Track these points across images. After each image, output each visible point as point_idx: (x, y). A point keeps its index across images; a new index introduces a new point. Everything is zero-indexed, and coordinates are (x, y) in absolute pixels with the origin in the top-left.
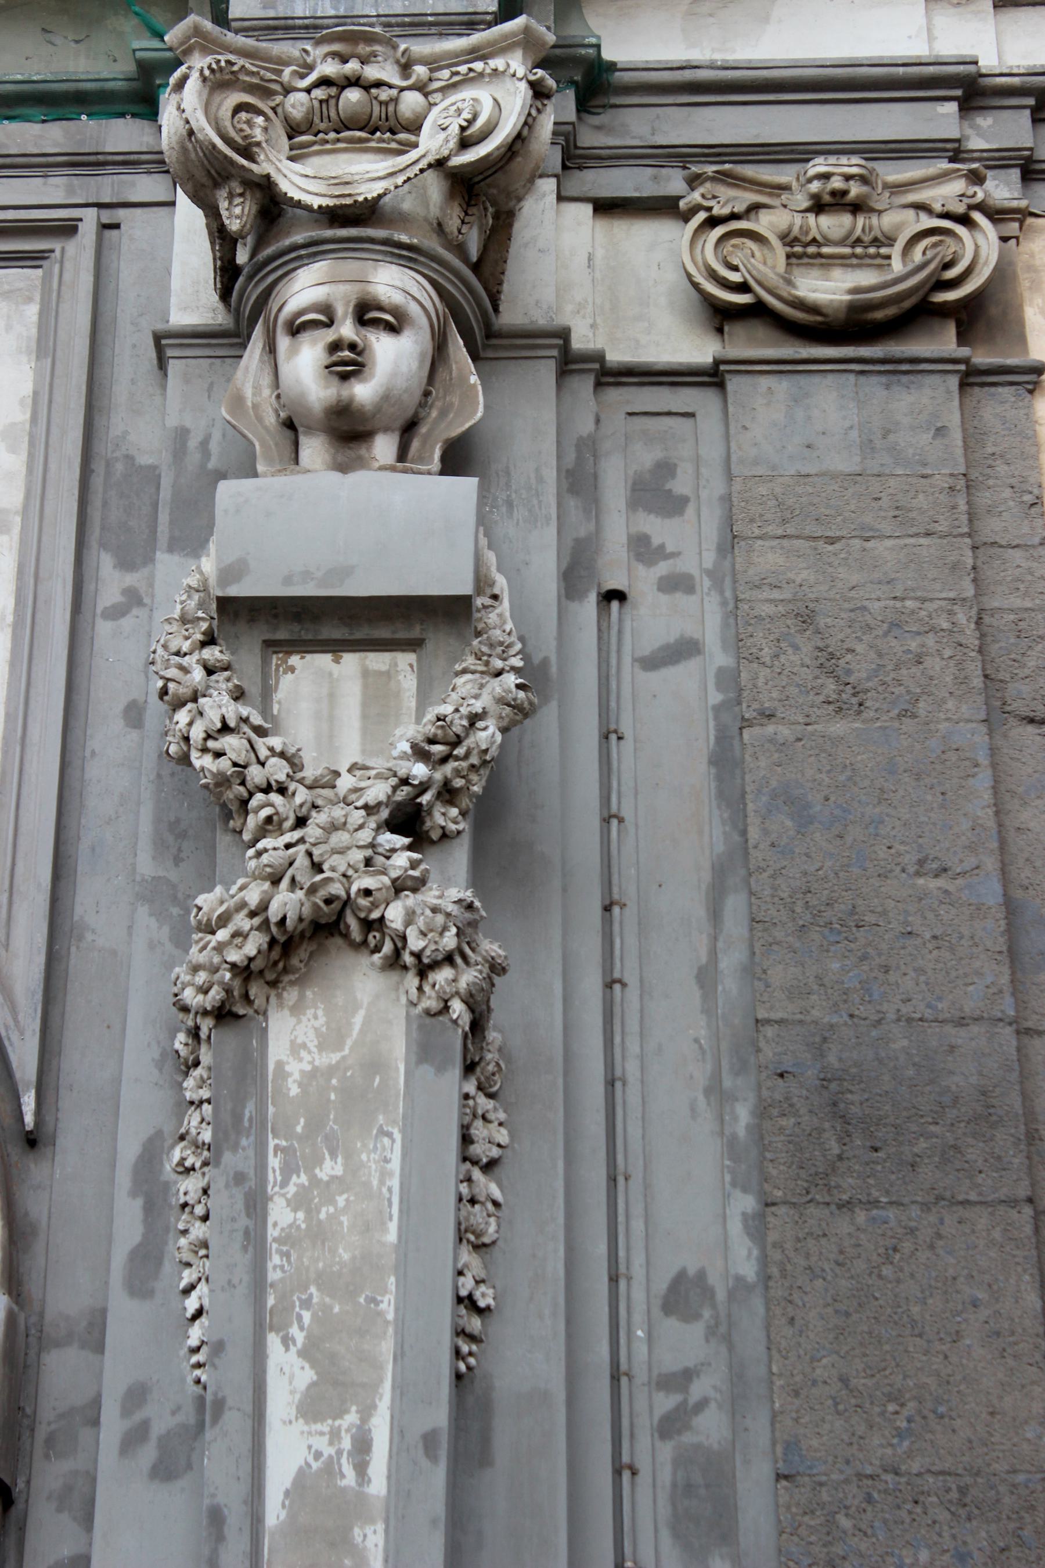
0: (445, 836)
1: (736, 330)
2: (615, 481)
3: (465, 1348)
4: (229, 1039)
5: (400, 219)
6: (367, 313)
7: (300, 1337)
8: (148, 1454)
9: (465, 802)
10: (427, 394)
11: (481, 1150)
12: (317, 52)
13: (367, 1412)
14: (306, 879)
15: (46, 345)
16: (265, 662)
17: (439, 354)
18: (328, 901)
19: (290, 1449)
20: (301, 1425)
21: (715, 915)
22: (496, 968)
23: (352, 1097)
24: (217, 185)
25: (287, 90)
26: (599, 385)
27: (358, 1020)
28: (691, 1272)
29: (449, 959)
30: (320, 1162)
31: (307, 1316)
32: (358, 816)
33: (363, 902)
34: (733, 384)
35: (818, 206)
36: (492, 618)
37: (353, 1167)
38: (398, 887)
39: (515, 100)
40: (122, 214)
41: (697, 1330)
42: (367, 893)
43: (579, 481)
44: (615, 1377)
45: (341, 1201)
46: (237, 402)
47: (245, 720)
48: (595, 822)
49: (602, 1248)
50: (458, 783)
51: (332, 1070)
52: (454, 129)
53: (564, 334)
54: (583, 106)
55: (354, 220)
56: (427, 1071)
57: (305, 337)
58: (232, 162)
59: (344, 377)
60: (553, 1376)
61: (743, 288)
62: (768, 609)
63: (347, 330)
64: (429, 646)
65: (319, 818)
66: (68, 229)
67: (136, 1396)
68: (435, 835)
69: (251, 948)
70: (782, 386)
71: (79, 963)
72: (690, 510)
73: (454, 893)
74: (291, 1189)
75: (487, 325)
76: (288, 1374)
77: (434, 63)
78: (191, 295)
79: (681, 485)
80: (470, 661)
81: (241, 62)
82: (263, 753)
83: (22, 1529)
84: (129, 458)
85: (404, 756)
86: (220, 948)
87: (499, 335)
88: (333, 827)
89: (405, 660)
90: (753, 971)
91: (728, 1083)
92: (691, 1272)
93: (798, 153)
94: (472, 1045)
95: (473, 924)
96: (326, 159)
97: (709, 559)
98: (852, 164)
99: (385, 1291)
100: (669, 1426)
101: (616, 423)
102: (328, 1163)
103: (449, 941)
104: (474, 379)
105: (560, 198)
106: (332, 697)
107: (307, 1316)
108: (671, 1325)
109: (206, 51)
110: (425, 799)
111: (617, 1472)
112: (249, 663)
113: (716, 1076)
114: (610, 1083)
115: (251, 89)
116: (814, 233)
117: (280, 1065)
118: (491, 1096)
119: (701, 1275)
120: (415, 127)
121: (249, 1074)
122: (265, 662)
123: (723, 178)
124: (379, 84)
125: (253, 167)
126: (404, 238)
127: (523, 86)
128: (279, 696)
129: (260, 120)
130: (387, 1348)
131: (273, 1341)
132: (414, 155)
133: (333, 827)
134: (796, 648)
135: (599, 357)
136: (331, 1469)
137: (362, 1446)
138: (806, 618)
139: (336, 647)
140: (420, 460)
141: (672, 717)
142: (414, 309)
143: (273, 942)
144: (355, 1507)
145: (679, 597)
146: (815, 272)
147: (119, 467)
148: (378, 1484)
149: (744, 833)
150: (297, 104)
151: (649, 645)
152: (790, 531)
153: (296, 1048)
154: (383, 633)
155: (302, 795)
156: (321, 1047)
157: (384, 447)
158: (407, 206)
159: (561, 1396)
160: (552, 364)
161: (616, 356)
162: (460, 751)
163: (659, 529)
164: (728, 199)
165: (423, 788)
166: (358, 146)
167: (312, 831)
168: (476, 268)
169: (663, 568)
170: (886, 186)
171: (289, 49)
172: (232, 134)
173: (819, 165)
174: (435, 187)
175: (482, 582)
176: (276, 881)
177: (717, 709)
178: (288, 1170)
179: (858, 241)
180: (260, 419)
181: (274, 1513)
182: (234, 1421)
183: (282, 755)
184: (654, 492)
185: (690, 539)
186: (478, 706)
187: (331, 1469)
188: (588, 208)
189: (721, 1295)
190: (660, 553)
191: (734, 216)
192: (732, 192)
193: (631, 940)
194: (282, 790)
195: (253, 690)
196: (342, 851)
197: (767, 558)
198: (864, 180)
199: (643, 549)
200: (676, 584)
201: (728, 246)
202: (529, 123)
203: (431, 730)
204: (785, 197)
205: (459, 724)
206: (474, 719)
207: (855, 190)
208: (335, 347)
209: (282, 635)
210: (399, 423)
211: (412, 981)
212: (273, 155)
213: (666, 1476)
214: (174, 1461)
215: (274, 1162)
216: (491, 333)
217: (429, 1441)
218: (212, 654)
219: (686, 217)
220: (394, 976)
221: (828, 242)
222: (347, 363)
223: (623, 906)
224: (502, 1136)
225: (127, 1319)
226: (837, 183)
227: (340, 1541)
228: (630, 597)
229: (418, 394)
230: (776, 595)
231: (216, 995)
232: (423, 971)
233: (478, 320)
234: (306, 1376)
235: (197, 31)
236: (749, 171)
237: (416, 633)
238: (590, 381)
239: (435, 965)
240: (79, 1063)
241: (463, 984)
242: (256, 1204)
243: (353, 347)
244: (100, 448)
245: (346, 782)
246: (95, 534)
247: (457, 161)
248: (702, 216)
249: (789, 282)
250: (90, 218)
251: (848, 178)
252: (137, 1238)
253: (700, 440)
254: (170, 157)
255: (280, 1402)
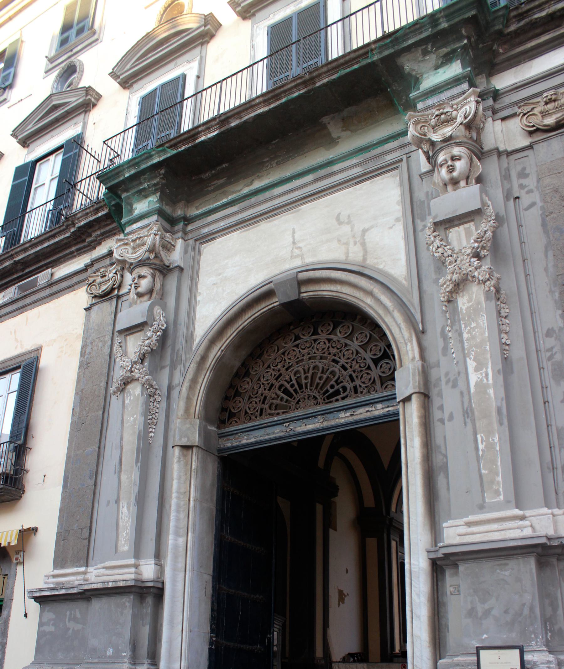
0: (485, 256)
1: (534, 135)
2: (514, 174)
3: (506, 353)
4: (451, 305)
5: (457, 137)
6: (453, 158)
7: (472, 357)
8: (450, 384)
9: (488, 248)
10: (470, 170)
11: (504, 314)
12: (434, 110)
13: (487, 369)
14: (458, 271)
15: (401, 184)
16: (445, 232)
17: (471, 160)
18: (464, 275)
19: (473, 378)
20: (475, 373)
21: (546, 256)
22: (498, 279)
23: (475, 311)
24: (421, 143)
25: (431, 120)
26: (508, 156)
27: (474, 296)
28: (550, 328)
29: (488, 280)
30: (471, 324)
31: (473, 353)
32: (466, 257)
33: (470, 273)
34: (535, 147)
35: (546, 103)
36: (488, 210)
37: (478, 324)
38: (476, 269)
39: (473, 105)
40: (411, 154)
41: (553, 339)
42: (471, 271)
43: (506, 176)
44: (537, 352)
45: (476, 330)
46: (434, 184)
47: (442, 245)
48: (519, 244)
49: (531, 328)
50: (485, 245)
51: (471, 306)
52: (463, 116)
53: (497, 149)
54: (495, 100)
55: (448, 141)
56: (488, 302)
57: (443, 167)
58: (421, 138)
59: (451, 172)
60: (523, 354)
61: (533, 126)
62: (549, 191)
63: (450, 163)
64: (476, 220)
65: (459, 259)
66: (401, 160)
67: (447, 374)
68: (483, 256)
69: (450, 288)
70: (545, 144)
71: (426, 297)
72: (530, 176)
73: (487, 267)
74: (467, 330)
75: (481, 152)
76: (471, 364)
77: (457, 104)
78: (425, 166)
79: (527, 171)
80: (484, 220)
81: (420, 118)
82: (446, 250)
83: (432, 401)
84: (420, 200)
85: (473, 243)
86: (445, 289)
87: (484, 153)
88: (462, 260)
89: (472, 224)
90: (556, 266)
91: (553, 289)
92: (550, 328)
93: (540, 94)
94: (497, 294)
95: (492, 272)
96: (441, 131)
97: (535, 184)
98: (552, 92)
99: (487, 345)
100: (549, 359)
101: (512, 163)
102: (473, 324)
103: (487, 276)
104: (479, 164)
105: (493, 121)
106: (460, 236)
107: (473, 353)
108: (548, 339)
109: (413, 118)
110: (479, 250)
111: (540, 369)
112: (442, 233)
113: (551, 288)
114: (529, 295)
115: (423, 122)
116: (547, 109)
117: (461, 308)
118: (504, 303)
119: (553, 328)
120: (456, 118)
121: (455, 311)
122: (445, 232)
123: (526, 105)
124: (447, 112)
125: (426, 137)
126: (458, 141)
127: (474, 102)
128: (450, 238)
129: (426, 128)
130: (489, 356)
131: (468, 359)
132: (456, 124)
133: (462, 260)
134: (555, 197)
135: (506, 151)
136: (482, 380)
137: (487, 375)
138: (557, 191)
139: (458, 225)
140: (471, 183)
141: (532, 219)
142: (462, 154)
143: (455, 285)
144: (487, 386)
145: (531, 194)
146: (549, 117)
147: (418, 202)
148: (491, 381)
149: (550, 238)
150: (433, 122)
151: (525, 207)
152: (551, 173)
153: (463, 304)
154: (466, 220)
155: (455, 256)
156: (468, 302)
157: (463, 183)
158: (458, 134)
159: (525, 357)
160: (496, 155)
161: (509, 149)
162: (484, 239)
163: (524, 181)
164: (526, 109)
165: (478, 248)
166: (447, 126)
167: (458, 262)
168: (476, 141)
169: (526, 189)
170: (561, 93)
171: (430, 112)
172: (421, 132)
173: (545, 95)
174: (462, 128)
175: (483, 204)
176: (453, 273)
177: (541, 215)
178: (466, 327)
179: (557, 108)
180: (439, 185)
181: (472, 390)
182: (463, 375)
183: (450, 249)
184: (523, 174)
185: (531, 182)
186: (486, 229)
187: (482, 380)
188: (500, 121)
189: (557, 331)
190: (526, 186)
191: (529, 112)
192: (527, 107)
193: (530, 266)
194: (451, 256)
195: (444, 238)
196: (464, 265)
197: (547, 181)
198: (555, 94)
199: (522, 187)
200: (530, 192)
201: (528, 119)
202: (477, 109)
203: (477, 236)
204: (539, 104)
205: (482, 234)
206: (485, 232)
207: (553, 97)
208: (448, 167)
209: (447, 226)
210: (465, 177)
211: (483, 286)
212: (429, 133)
213: (550, 368)
214: (455, 385)
215: (463, 326)
216: (482, 153)
217: (499, 371)
218: (435, 234)
219: (519, 115)
220: (480, 286)
221: (550, 110)
222: (451, 169)
223: (527, 260)
224: (508, 311)
225: (443, 361)
226: (549, 97)
227: (485, 393)
228: (520, 197)
229: (468, 171)
230: (550, 188)
231: (446, 298)
232: (484, 283)
233: (479, 152)
234: (475, 364)
235: (410, 115)
236: (531, 101)
237: (472, 218)
238: (505, 156)
239: (485, 282)
240: (428, 317)
241: (492, 284)
242: (461, 335)
243: (451, 166)
244: (415, 200)
245: (463, 251)
246: (416, 217)
247: (464, 122)
248: (522, 114)
249: (542, 122)
250: (404, 157)
251: (551, 95)
252: (443, 346)
253: (531, 161)
254: (411, 141)
255: (471, 370)
